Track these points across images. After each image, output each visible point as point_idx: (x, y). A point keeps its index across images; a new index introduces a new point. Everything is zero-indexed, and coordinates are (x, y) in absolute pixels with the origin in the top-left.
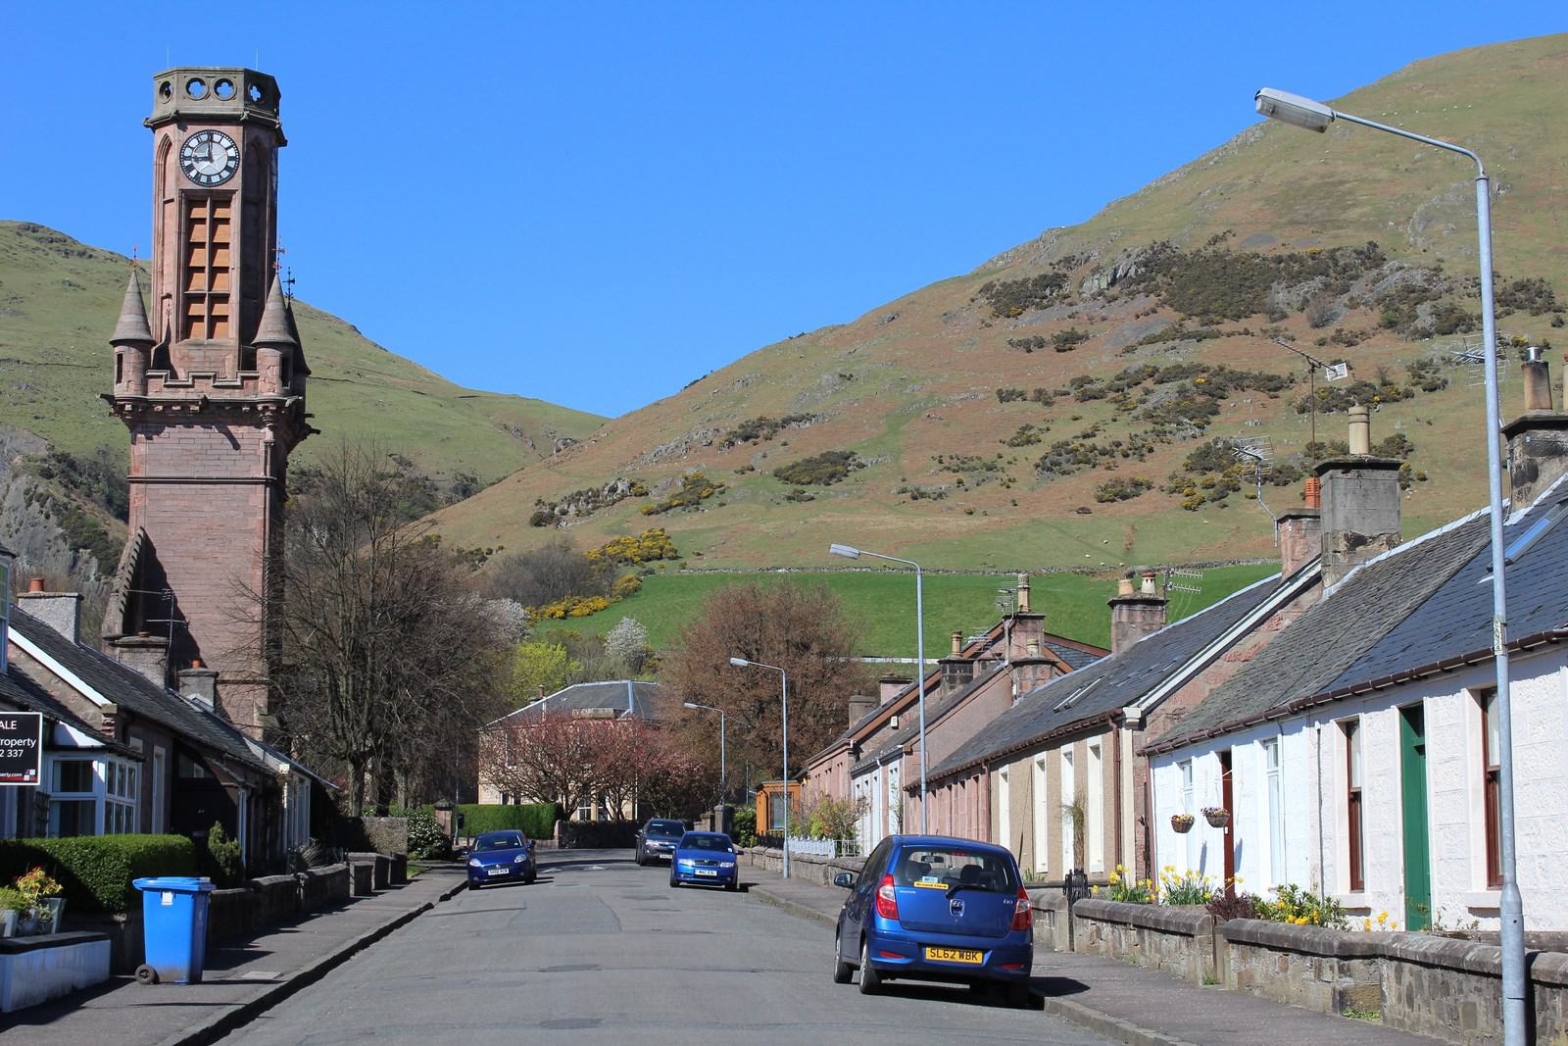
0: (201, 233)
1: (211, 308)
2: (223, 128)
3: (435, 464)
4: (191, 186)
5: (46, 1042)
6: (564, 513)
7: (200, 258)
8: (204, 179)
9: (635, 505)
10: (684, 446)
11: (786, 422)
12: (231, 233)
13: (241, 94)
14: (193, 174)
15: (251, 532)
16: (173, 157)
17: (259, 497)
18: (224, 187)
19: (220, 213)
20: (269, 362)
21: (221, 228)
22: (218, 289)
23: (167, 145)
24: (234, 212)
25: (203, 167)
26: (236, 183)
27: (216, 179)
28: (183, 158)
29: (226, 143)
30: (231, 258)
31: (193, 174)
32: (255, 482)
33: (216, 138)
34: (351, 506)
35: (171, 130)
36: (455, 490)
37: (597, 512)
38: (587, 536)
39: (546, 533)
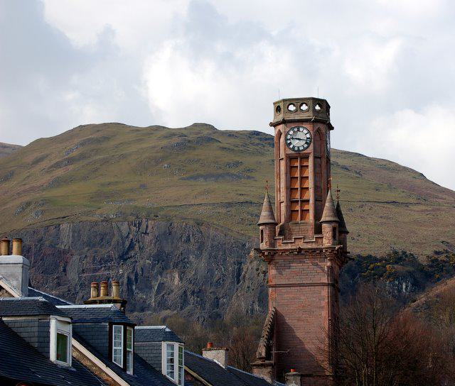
1: (301, 207)
2: (306, 125)
4: (290, 152)
8: (296, 149)
13: (311, 109)
14: (291, 146)
15: (323, 307)
20: (327, 230)
24: (310, 163)
25: (295, 143)
26: (311, 149)
28: (286, 139)
29: (305, 131)
30: (310, 184)
31: (291, 146)
32: (323, 285)
33: (301, 129)
34: (421, 269)
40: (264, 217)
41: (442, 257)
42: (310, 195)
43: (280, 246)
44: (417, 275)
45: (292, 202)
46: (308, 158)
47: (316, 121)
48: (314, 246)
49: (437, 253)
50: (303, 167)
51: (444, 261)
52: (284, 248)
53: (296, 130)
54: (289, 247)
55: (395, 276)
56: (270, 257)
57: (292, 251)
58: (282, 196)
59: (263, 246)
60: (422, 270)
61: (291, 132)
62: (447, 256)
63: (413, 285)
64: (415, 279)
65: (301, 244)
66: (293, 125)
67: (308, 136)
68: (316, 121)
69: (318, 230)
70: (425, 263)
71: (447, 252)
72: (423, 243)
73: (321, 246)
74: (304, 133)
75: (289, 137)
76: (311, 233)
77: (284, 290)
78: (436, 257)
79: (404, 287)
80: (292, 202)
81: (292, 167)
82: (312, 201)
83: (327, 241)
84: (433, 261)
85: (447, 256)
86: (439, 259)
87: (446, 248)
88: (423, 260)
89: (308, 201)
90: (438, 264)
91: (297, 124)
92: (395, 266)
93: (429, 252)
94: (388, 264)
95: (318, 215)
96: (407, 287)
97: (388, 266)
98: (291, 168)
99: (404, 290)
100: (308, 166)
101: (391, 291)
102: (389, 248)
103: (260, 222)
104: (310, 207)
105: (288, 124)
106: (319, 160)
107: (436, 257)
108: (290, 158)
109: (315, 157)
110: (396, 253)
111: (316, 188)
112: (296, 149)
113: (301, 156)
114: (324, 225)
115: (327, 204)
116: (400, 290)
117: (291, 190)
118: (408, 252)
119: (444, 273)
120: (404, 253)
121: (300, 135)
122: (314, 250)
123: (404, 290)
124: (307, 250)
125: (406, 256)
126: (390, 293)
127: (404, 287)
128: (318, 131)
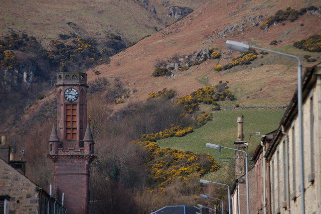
0: (70, 113)
1: (72, 132)
2: (75, 87)
3: (97, 28)
4: (67, 102)
5: (319, 174)
6: (173, 68)
7: (70, 119)
8: (70, 100)
9: (214, 64)
10: (242, 27)
11: (304, 11)
12: (77, 113)
13: (78, 79)
14: (67, 99)
15: (83, 187)
16: (62, 94)
17: (85, 178)
18: (75, 102)
19: (74, 108)
20: (87, 146)
21: (74, 117)
22: (74, 127)
23: (61, 91)
24: (78, 107)
25: (70, 97)
26: (78, 101)
27: (73, 100)
28: (65, 95)
29: (75, 91)
30: (77, 119)
31: (67, 99)
32: (84, 174)
33: (73, 89)
34: (45, 56)
35: (61, 88)
36: (109, 45)
37: (191, 68)
38: (185, 84)
39: (162, 84)
40: (52, 137)
41: (69, 42)
42: (77, 125)
43: (61, 153)
44: (41, 64)
45: (67, 129)
46: (76, 105)
47: (82, 85)
48: (79, 154)
49: (63, 37)
50: (74, 110)
51: (71, 47)
52: (63, 154)
53: (70, 89)
54: (66, 154)
55: (17, 65)
56: (56, 159)
57: (67, 156)
58: (61, 125)
59: (52, 153)
60: (45, 58)
61: (67, 91)
62: (74, 42)
63: (35, 74)
64: (38, 68)
65: (72, 153)
66: (68, 87)
67: (77, 93)
68: (82, 85)
69: (81, 145)
70: (49, 49)
71: (74, 36)
72: (46, 24)
73: (83, 154)
74: (74, 92)
75: (66, 93)
76: (77, 146)
77: (62, 177)
78: (62, 41)
79: (25, 76)
80: (67, 129)
81: (67, 110)
82: (78, 129)
83: (86, 152)
84: (58, 47)
85: (74, 42)
86: (66, 44)
87: (73, 31)
88: (46, 45)
89: (76, 129)
90: (65, 51)
91: (70, 87)
92: (15, 52)
93: (54, 35)
94: (6, 49)
95: (81, 137)
96: (28, 77)
97: (5, 52)
98: (66, 110)
99: (25, 80)
100: (76, 109)
101: (10, 80)
102: (7, 30)
103: (50, 140)
104: (77, 131)
105: (66, 87)
106: (82, 106)
107: (62, 41)
108: (67, 105)
109: (80, 105)
110: (15, 36)
111: (81, 121)
112: (70, 100)
113: (71, 104)
114: (85, 143)
115: (87, 131)
116: (20, 80)
117: (66, 122)
118: (29, 35)
119: (71, 62)
120: (25, 36)
121: (72, 93)
122: (79, 156)
123: (25, 80)
124: (76, 156)
125: (27, 40)
126: (8, 83)
127: (25, 76)
128: (82, 90)
